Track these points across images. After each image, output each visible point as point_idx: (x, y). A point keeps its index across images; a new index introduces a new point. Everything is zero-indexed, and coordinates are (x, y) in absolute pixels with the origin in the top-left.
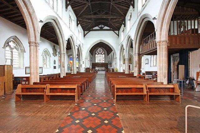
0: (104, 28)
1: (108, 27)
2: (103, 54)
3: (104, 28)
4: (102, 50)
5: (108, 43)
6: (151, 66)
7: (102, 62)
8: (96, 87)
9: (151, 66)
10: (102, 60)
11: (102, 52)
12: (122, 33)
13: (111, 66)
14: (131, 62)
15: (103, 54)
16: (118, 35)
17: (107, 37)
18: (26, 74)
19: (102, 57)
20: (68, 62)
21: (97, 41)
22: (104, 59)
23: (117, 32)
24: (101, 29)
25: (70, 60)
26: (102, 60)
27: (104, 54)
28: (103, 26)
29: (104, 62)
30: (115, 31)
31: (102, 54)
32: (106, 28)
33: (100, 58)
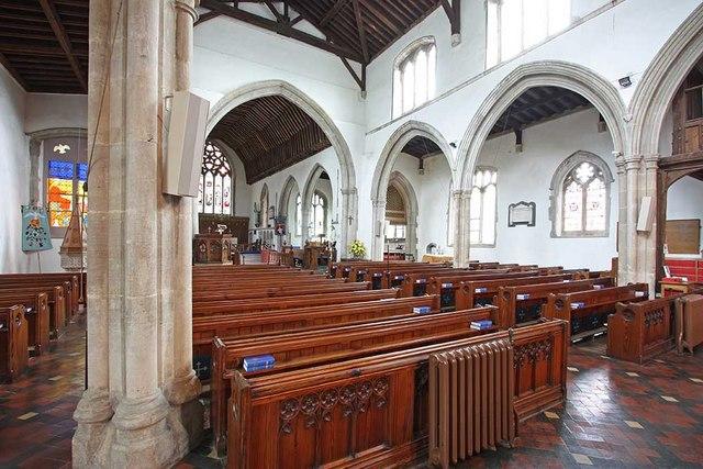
0: (295, 27)
1: (317, 24)
2: (223, 176)
3: (295, 27)
4: (218, 154)
5: (320, 111)
6: (553, 235)
7: (218, 211)
8: (607, 383)
9: (553, 235)
10: (218, 201)
11: (218, 162)
12: (397, 73)
13: (280, 230)
14: (403, 216)
15: (223, 176)
16: (363, 86)
17: (313, 78)
18: (533, 225)
19: (218, 189)
20: (33, 189)
21: (265, 84)
22: (228, 200)
23: (357, 66)
24: (283, 27)
25: (49, 175)
26: (218, 201)
27: (229, 173)
28: (293, 15)
29: (227, 211)
30: (350, 62)
31: (217, 171)
32: (305, 27)
33: (209, 191)
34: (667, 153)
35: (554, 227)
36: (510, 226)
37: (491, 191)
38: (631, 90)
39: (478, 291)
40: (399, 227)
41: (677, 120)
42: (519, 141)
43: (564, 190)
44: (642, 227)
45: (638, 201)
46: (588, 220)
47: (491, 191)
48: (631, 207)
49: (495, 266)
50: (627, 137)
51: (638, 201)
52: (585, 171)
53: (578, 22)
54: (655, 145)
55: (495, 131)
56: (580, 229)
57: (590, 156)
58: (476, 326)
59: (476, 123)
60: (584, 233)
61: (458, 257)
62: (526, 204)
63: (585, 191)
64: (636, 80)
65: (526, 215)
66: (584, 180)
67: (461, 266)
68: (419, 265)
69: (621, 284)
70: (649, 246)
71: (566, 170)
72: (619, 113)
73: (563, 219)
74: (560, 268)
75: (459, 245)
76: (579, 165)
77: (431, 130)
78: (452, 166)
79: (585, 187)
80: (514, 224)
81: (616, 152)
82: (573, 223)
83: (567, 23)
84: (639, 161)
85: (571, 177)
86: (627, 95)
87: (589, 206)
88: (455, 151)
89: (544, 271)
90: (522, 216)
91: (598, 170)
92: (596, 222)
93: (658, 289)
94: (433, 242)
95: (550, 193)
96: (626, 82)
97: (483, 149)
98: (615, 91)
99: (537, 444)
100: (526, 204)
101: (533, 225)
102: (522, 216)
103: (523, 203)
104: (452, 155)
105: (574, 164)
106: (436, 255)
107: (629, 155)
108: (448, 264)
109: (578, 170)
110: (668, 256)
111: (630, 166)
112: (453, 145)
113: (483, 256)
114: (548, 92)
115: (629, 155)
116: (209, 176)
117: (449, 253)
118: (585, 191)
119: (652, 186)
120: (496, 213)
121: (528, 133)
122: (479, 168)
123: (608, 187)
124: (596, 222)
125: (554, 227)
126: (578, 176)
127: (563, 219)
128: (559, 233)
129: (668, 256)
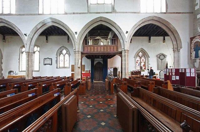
2: (141, 58)
9: (57, 68)
18: (52, 65)
34: (82, 51)
35: (57, 65)
36: (44, 65)
37: (37, 53)
38: (77, 35)
39: (44, 85)
40: (174, 79)
41: (84, 44)
42: (47, 39)
43: (59, 56)
44: (79, 66)
45: (78, 60)
46: (65, 64)
47: (37, 53)
48: (77, 61)
49: (40, 77)
50: (76, 46)
51: (78, 60)
52: (64, 52)
53: (66, 14)
54: (81, 50)
55: (42, 34)
56: (63, 66)
57: (66, 48)
58: (30, 95)
59: (35, 30)
60: (64, 67)
61: (28, 75)
62: (49, 59)
63: (64, 57)
64: (78, 33)
65: (49, 62)
66: (64, 54)
67: (29, 78)
68: (6, 80)
69: (75, 79)
70: (80, 70)
71: (60, 50)
72: (75, 40)
73: (59, 63)
74: (59, 76)
75: (28, 71)
76: (63, 50)
77: (14, 26)
78: (25, 43)
79: (64, 56)
80: (46, 64)
81: (74, 49)
82: (61, 65)
83: (64, 13)
84: (78, 51)
85: (61, 53)
86: (76, 36)
87: (65, 61)
88: (26, 38)
89: (49, 78)
90: (47, 62)
91: (67, 52)
92: (67, 65)
93: (81, 79)
94: (12, 70)
95: (56, 56)
96: (76, 33)
97: (37, 40)
98: (79, 34)
99: (78, 124)
100: (49, 59)
101: (52, 65)
102: (47, 62)
103: (48, 58)
104: (25, 39)
105: (62, 49)
106: (14, 75)
107: (77, 50)
108: (23, 79)
109: (63, 51)
110: (83, 72)
111: (77, 52)
112: (26, 35)
113: (35, 75)
114: (56, 28)
115: (77, 50)
116: (138, 59)
117: (24, 74)
118: (64, 57)
119: (80, 57)
120: (40, 61)
121: (50, 38)
122: (35, 45)
123: (69, 56)
124: (67, 65)
125: (57, 65)
126: (63, 53)
127: (59, 63)
128: (58, 67)
129: (83, 72)
